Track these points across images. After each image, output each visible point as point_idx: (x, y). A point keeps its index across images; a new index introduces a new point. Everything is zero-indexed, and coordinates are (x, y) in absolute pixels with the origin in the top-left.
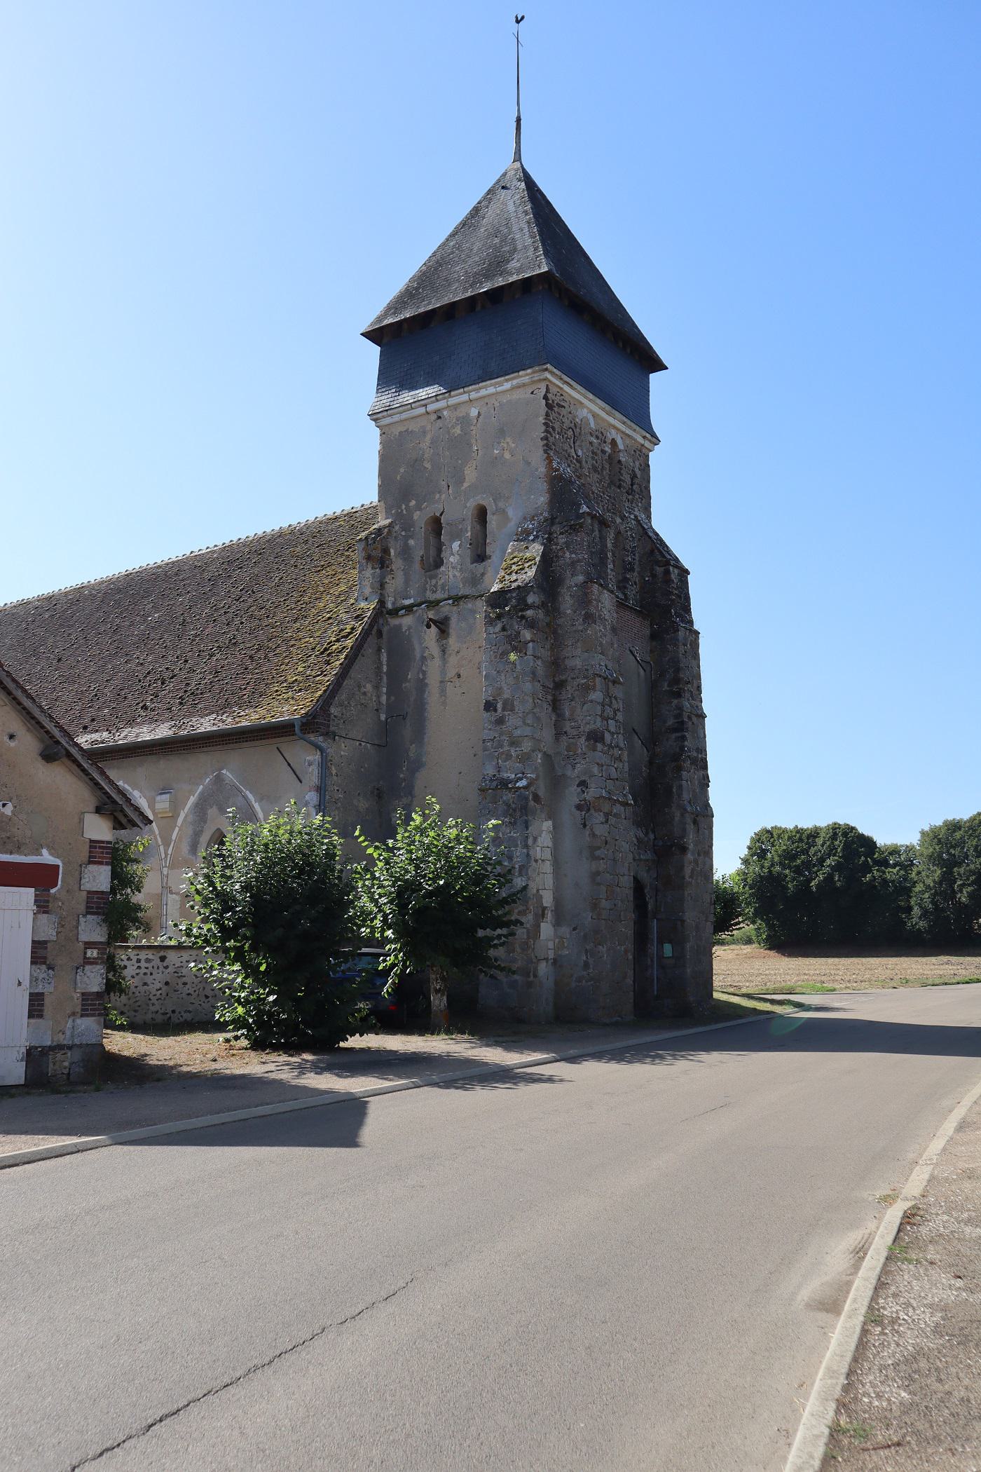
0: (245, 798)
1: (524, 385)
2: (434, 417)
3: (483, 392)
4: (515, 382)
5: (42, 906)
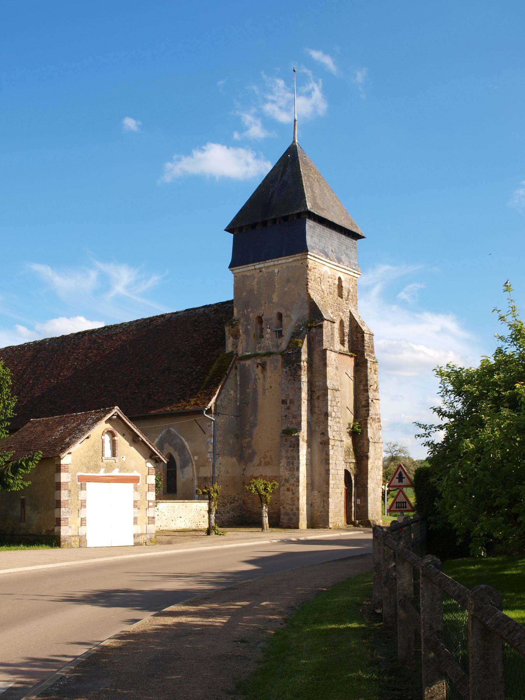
0: (181, 439)
1: (298, 260)
2: (258, 271)
3: (280, 262)
4: (294, 259)
5: (136, 489)
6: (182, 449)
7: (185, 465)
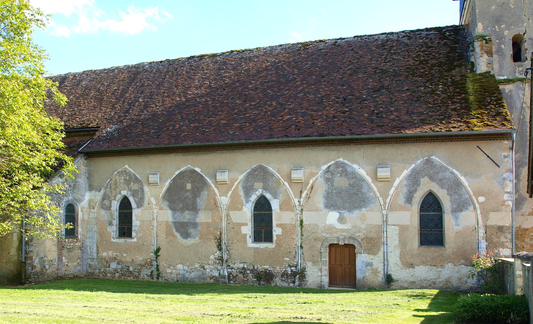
0: (452, 173)
6: (455, 186)
7: (461, 206)
